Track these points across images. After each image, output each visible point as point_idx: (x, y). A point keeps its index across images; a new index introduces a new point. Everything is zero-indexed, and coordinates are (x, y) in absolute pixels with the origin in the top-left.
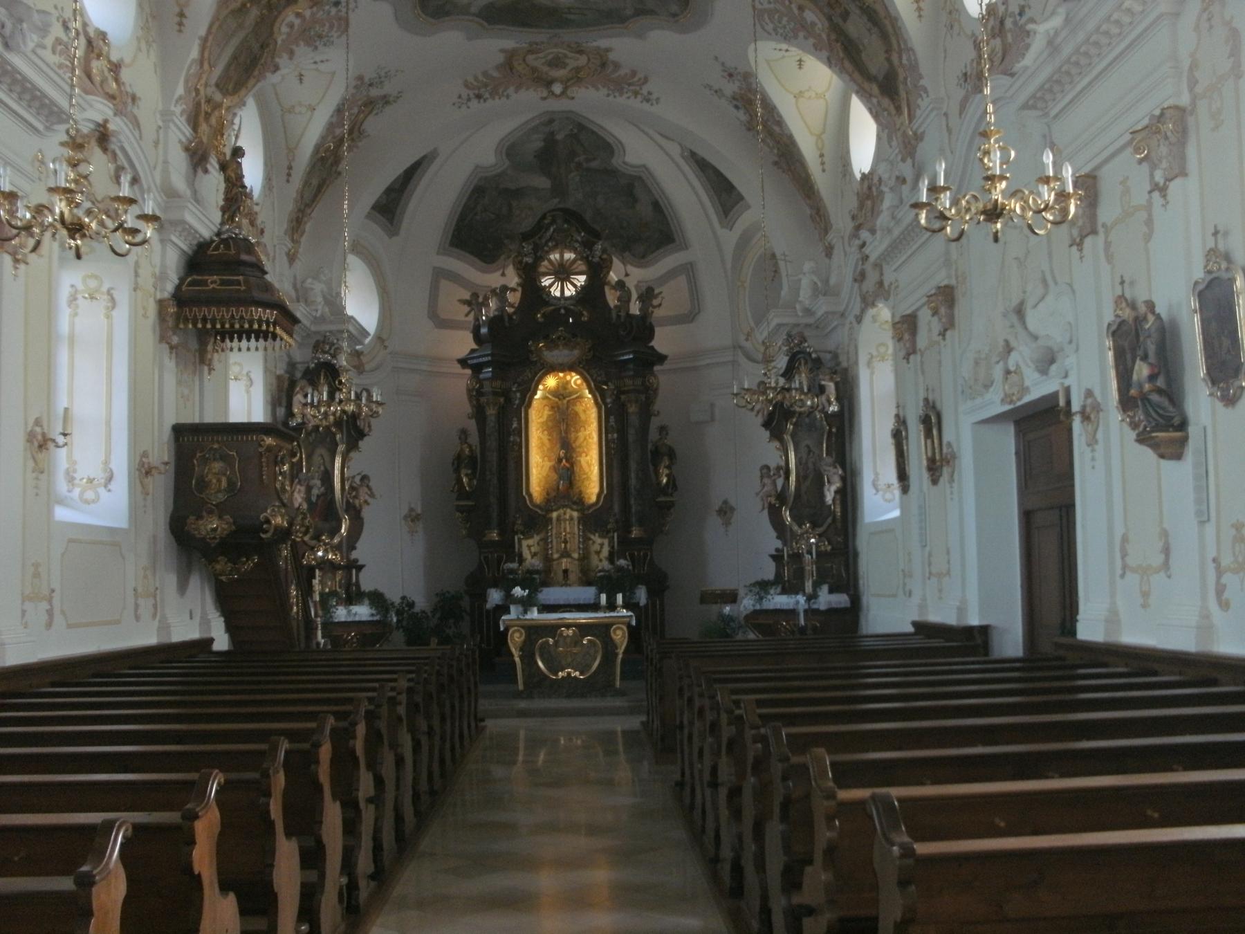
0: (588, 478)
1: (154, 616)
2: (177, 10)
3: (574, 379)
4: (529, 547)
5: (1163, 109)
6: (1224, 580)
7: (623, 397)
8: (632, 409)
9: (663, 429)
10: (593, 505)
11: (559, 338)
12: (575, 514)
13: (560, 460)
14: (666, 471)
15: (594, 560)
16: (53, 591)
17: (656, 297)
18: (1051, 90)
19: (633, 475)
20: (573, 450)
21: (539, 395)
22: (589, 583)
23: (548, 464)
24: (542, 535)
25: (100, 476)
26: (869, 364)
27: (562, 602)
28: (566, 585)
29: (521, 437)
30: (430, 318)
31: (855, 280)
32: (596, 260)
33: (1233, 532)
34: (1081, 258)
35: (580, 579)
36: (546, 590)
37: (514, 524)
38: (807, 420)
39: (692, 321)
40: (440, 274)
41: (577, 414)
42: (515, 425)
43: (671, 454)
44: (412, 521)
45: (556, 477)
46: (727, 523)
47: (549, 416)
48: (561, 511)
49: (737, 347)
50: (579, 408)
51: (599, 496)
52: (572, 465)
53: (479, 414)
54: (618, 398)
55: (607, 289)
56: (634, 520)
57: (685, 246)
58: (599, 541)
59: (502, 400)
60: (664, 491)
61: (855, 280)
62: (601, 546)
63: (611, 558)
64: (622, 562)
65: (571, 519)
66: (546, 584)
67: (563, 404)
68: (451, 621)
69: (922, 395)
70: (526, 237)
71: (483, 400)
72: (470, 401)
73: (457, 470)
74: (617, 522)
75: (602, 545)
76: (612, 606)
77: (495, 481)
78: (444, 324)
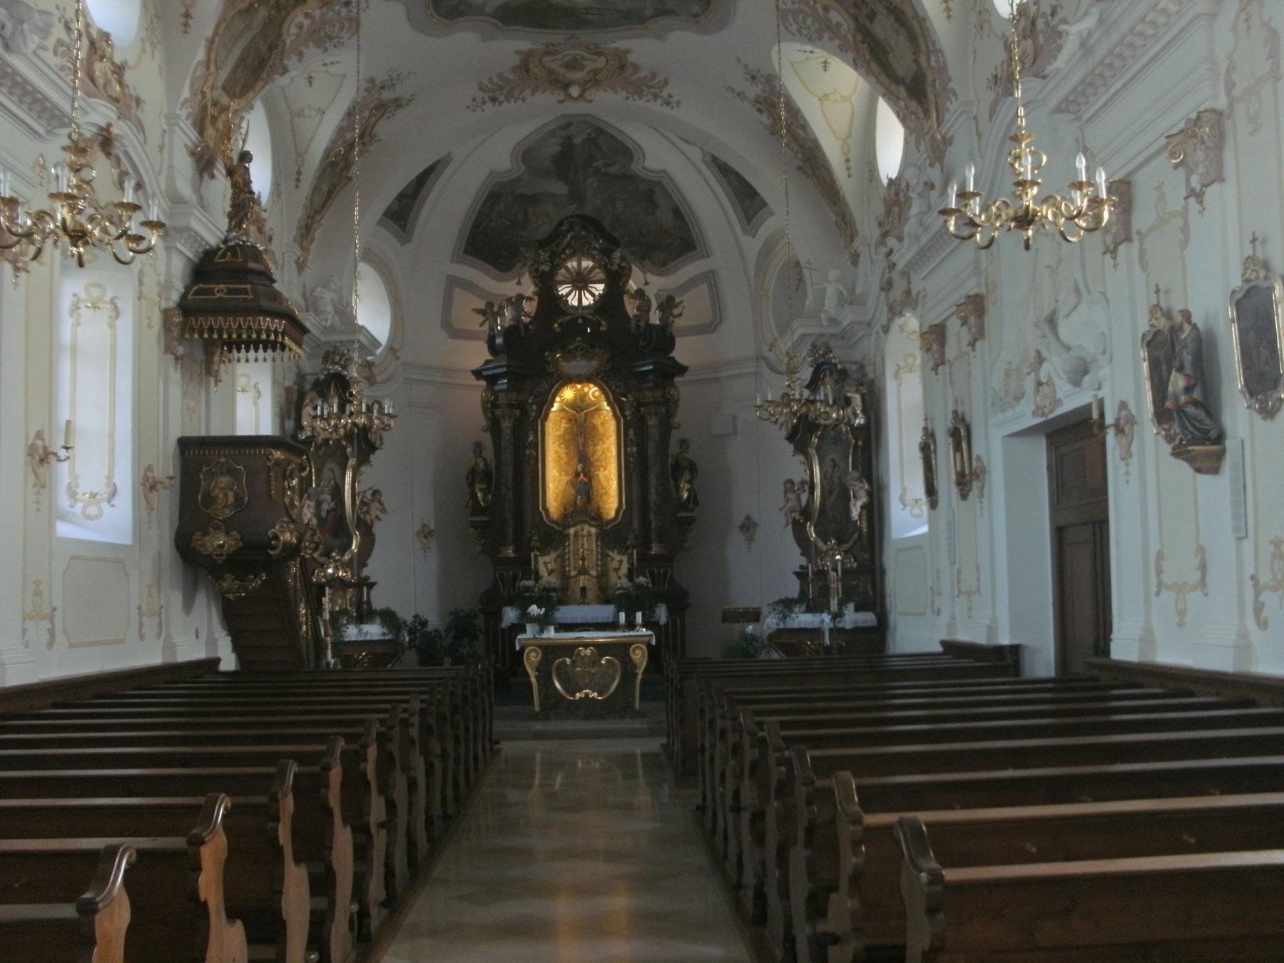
0: (607, 493)
1: (159, 635)
2: (183, 10)
3: (592, 391)
4: (546, 564)
5: (1200, 113)
6: (1262, 598)
7: (642, 409)
8: (652, 421)
9: (684, 443)
10: (612, 521)
11: (576, 348)
12: (593, 530)
13: (577, 475)
14: (687, 486)
15: (613, 578)
17: (676, 306)
18: (1083, 93)
19: (653, 490)
20: (591, 464)
21: (556, 407)
22: (607, 601)
23: (565, 479)
24: (559, 552)
25: (103, 490)
26: (896, 375)
27: (579, 621)
28: (584, 603)
29: (537, 450)
30: (443, 328)
31: (882, 289)
32: (615, 268)
33: (1272, 548)
34: (1115, 266)
35: (598, 596)
36: (563, 608)
37: (530, 540)
38: (832, 433)
39: (713, 331)
40: (453, 283)
41: (595, 427)
42: (531, 438)
43: (692, 468)
44: (425, 537)
45: (573, 491)
46: (750, 540)
47: (566, 429)
48: (579, 527)
49: (760, 357)
50: (597, 421)
51: (618, 511)
52: (590, 479)
53: (494, 427)
54: (637, 410)
55: (626, 298)
56: (654, 536)
57: (706, 254)
58: (618, 557)
59: (518, 412)
60: (684, 506)
61: (882, 289)
62: (620, 563)
63: (630, 576)
64: (642, 580)
65: (589, 535)
66: (563, 602)
67: (580, 417)
68: (466, 640)
69: (951, 407)
70: (542, 244)
71: (498, 412)
72: (485, 414)
73: (471, 485)
74: (636, 538)
75: (620, 562)
76: (631, 625)
77: (511, 496)
78: (458, 334)
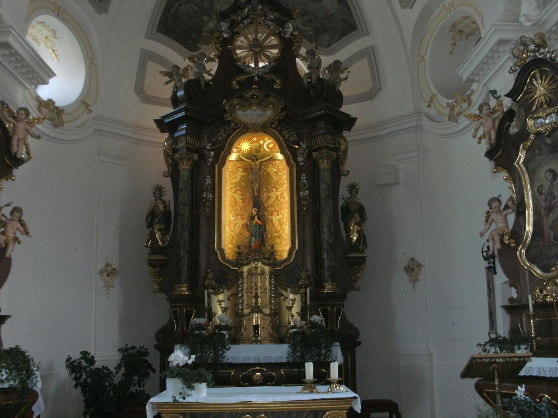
0: (280, 236)
3: (267, 143)
4: (220, 302)
7: (314, 154)
8: (324, 165)
9: (353, 188)
10: (285, 261)
11: (252, 96)
12: (267, 269)
13: (252, 218)
14: (357, 228)
15: (286, 317)
17: (342, 72)
19: (325, 230)
20: (266, 209)
21: (233, 157)
22: (281, 341)
23: (240, 222)
24: (233, 291)
27: (251, 361)
28: (256, 342)
29: (214, 194)
32: (287, 36)
35: (271, 335)
36: (234, 347)
37: (205, 279)
38: (549, 141)
39: (373, 98)
40: (146, 56)
41: (269, 175)
42: (208, 181)
43: (361, 211)
44: (108, 275)
45: (248, 234)
46: (414, 280)
47: (243, 177)
48: (253, 265)
49: (418, 113)
50: (271, 170)
51: (290, 252)
52: (264, 223)
53: (174, 173)
54: (309, 156)
55: (298, 60)
56: (326, 274)
57: (366, 32)
58: (292, 296)
59: (196, 156)
60: (355, 247)
62: (293, 305)
63: (303, 314)
64: (316, 318)
65: (263, 273)
66: (235, 341)
67: (255, 165)
68: (136, 378)
70: (223, 16)
71: (177, 156)
72: (166, 161)
73: (150, 225)
74: (308, 277)
75: (294, 300)
76: (322, 378)
77: (186, 235)
78: (148, 100)
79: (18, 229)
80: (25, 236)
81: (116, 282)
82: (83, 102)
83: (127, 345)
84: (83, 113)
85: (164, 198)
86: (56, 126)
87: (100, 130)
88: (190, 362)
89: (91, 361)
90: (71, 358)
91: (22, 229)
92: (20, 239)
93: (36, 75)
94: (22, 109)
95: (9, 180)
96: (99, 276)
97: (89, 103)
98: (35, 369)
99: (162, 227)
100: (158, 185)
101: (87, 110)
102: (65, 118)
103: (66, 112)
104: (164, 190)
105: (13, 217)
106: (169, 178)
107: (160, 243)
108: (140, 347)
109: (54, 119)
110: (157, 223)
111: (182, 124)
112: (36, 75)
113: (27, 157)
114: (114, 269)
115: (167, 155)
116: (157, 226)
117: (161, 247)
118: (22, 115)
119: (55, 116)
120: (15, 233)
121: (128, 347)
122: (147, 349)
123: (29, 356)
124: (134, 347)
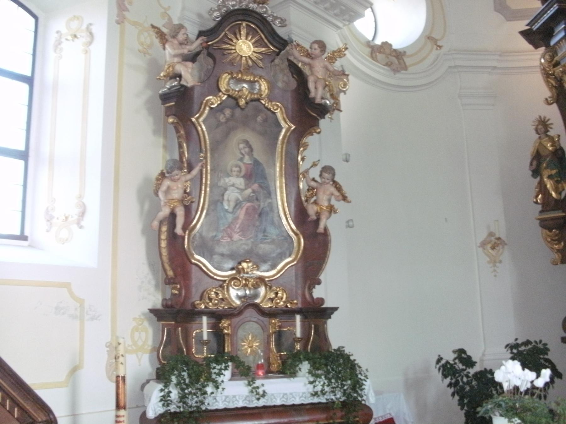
16: (119, 344)
25: (74, 212)
30: (496, 10)
44: (493, 248)
72: (547, 82)
73: (536, 172)
79: (332, 194)
80: (342, 202)
81: (506, 255)
82: (429, 38)
83: (516, 339)
84: (431, 51)
85: (551, 133)
86: (396, 71)
87: (456, 67)
88: (540, 383)
89: (469, 362)
90: (442, 359)
91: (337, 193)
92: (336, 207)
93: (344, 8)
94: (316, 42)
95: (314, 134)
96: (480, 250)
97: (437, 37)
98: (363, 378)
99: (554, 172)
100: (540, 117)
101: (435, 47)
102: (408, 61)
103: (408, 53)
104: (549, 122)
105: (323, 180)
106: (555, 106)
107: (554, 194)
108: (536, 342)
109: (392, 63)
110: (547, 168)
111: (558, 24)
112: (344, 8)
113: (332, 101)
114: (499, 239)
115: (547, 75)
116: (546, 173)
117: (556, 200)
118: (315, 49)
119: (395, 60)
120: (329, 200)
121: (519, 342)
122: (545, 344)
123: (355, 360)
124: (528, 343)
